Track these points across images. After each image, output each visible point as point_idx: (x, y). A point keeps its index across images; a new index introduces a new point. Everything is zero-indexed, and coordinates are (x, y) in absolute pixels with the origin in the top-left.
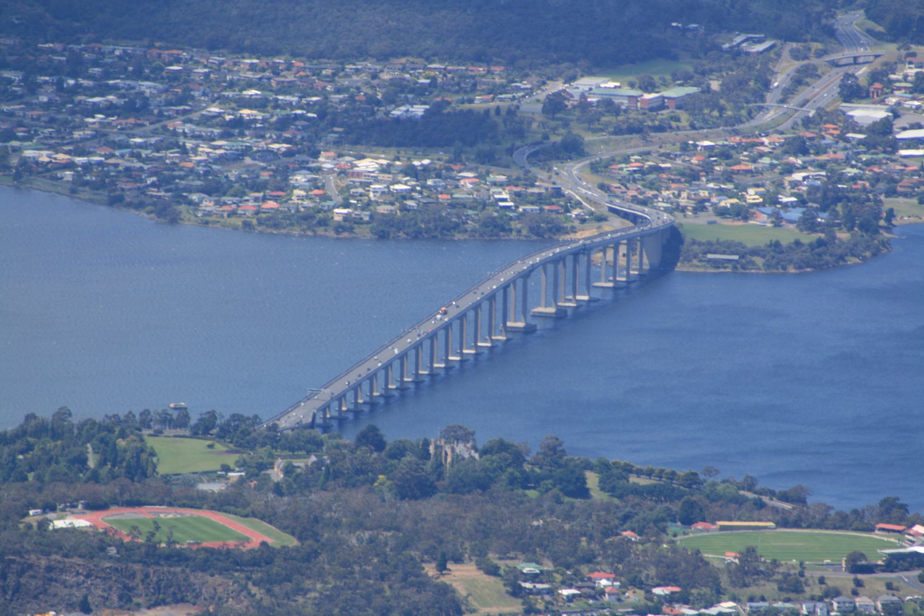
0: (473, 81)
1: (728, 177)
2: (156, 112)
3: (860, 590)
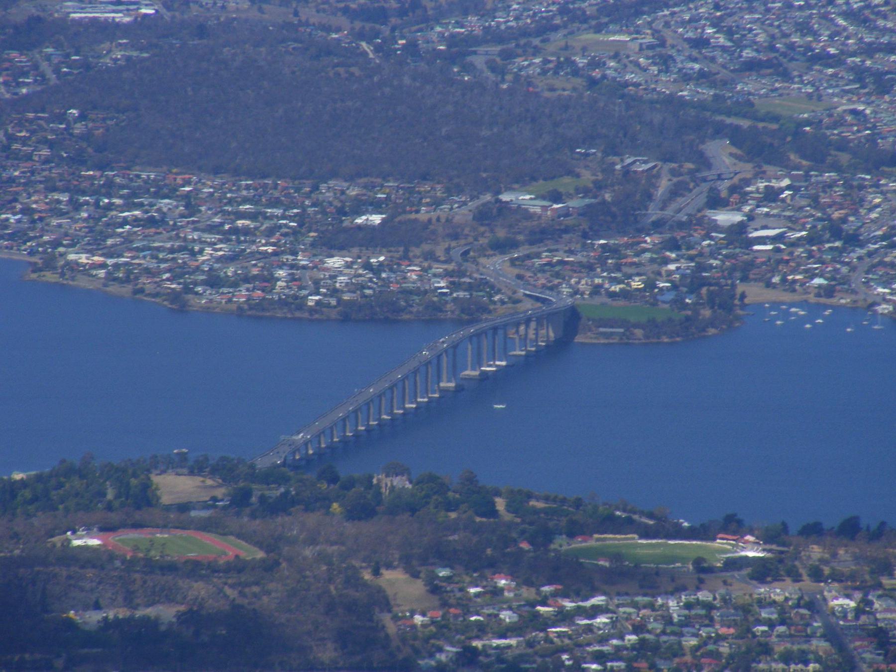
0: (419, 196)
1: (618, 268)
2: (171, 223)
3: (702, 586)
